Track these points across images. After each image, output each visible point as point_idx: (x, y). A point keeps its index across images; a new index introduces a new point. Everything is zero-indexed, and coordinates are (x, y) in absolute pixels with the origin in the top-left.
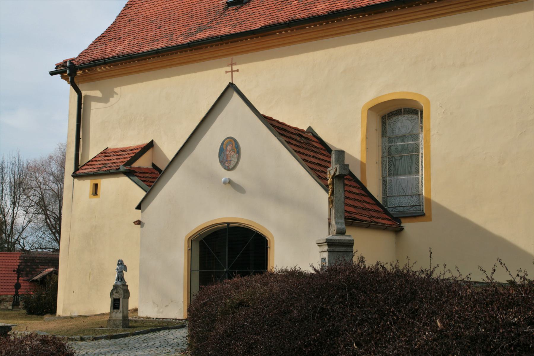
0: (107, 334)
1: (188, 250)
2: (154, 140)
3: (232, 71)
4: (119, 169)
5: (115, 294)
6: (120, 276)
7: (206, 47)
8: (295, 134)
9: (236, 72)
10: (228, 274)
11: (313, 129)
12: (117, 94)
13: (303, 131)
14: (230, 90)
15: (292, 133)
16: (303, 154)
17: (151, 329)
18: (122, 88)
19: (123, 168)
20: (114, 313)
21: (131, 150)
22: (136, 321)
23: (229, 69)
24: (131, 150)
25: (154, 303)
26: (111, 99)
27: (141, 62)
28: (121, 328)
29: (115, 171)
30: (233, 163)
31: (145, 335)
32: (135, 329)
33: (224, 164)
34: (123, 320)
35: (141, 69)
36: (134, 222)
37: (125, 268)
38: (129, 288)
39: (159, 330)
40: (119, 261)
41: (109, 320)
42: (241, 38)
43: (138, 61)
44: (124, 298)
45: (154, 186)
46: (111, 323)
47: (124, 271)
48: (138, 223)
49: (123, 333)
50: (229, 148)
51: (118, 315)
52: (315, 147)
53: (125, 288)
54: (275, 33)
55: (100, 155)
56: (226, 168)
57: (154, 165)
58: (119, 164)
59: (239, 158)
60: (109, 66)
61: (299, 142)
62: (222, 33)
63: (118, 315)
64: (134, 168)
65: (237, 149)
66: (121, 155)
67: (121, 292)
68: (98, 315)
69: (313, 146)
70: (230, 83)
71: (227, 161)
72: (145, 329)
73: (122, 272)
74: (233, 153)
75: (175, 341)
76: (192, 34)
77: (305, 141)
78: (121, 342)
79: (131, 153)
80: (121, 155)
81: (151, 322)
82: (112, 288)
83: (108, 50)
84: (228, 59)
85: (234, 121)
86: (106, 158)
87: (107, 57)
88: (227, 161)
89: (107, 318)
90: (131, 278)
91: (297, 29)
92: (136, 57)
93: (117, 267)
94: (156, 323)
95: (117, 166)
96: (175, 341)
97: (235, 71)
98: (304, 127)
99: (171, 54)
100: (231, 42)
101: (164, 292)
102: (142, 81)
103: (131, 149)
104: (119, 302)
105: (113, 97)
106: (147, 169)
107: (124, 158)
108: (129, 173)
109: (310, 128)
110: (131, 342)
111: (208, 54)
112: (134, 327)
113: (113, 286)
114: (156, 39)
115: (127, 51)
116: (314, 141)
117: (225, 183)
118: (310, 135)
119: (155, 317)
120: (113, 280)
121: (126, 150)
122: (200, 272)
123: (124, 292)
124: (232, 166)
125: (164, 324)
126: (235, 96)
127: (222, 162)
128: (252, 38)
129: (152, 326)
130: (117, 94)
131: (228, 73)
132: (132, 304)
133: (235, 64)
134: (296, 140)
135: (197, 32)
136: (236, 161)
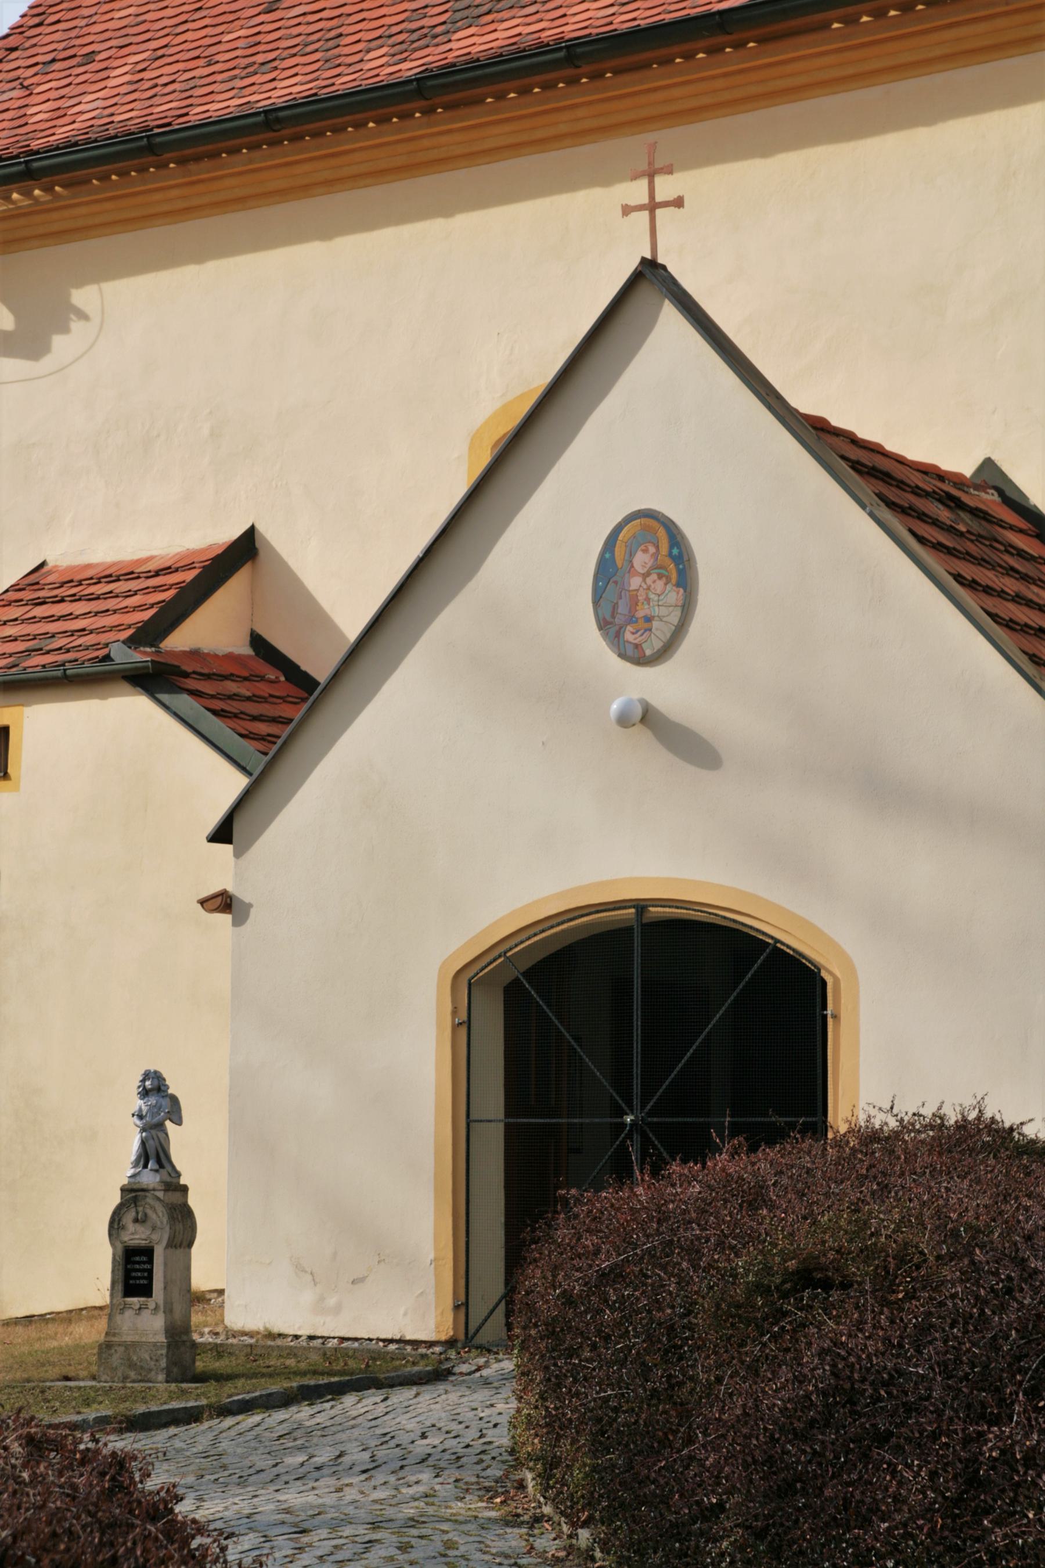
0: (105, 1410)
1: (456, 1027)
2: (260, 527)
3: (652, 206)
4: (107, 658)
5: (131, 1227)
6: (151, 1145)
7: (500, 97)
8: (927, 494)
9: (671, 209)
10: (644, 1136)
11: (1006, 468)
12: (83, 316)
13: (957, 480)
14: (646, 293)
15: (917, 491)
16: (988, 590)
17: (301, 1387)
18: (108, 287)
19: (125, 656)
20: (129, 1313)
21: (157, 574)
22: (219, 1351)
23: (637, 191)
24: (157, 574)
25: (299, 1268)
26: (58, 341)
27: (192, 167)
28: (160, 1385)
29: (88, 669)
30: (661, 631)
31: (281, 1415)
32: (228, 1387)
33: (618, 635)
34: (169, 1346)
35: (196, 201)
36: (203, 902)
37: (175, 1112)
38: (193, 1201)
39: (337, 1391)
40: (147, 1075)
41: (106, 1347)
42: (663, 52)
43: (181, 162)
44: (172, 1244)
45: (292, 736)
46: (116, 1359)
47: (168, 1124)
48: (223, 903)
49: (175, 1405)
50: (641, 560)
51: (148, 1324)
52: (1021, 554)
53: (175, 1197)
54: (826, 26)
55: (13, 596)
56: (630, 651)
57: (258, 642)
58: (104, 638)
59: (687, 608)
60: (48, 189)
61: (950, 530)
62: (571, 29)
63: (148, 1324)
64: (172, 653)
65: (678, 561)
66: (110, 595)
67: (159, 1215)
68: (17, 1321)
69: (1011, 549)
70: (644, 260)
71: (631, 619)
72: (275, 1387)
73: (160, 1126)
74: (660, 585)
75: (434, 1440)
76: (430, 36)
77: (976, 526)
78: (178, 1444)
79: (156, 589)
80: (110, 595)
81: (292, 1353)
82: (116, 1199)
83: (39, 113)
84: (632, 146)
85: (665, 436)
86: (39, 611)
87: (35, 145)
88: (631, 619)
89: (91, 1333)
90: (197, 1152)
91: (760, 41)
92: (167, 146)
93: (138, 1103)
94: (314, 1357)
95: (96, 646)
96: (434, 1440)
97: (666, 204)
98: (966, 466)
99: (335, 130)
100: (617, 72)
101: (349, 1220)
102: (199, 258)
103: (152, 566)
104: (151, 1261)
105: (65, 330)
106: (230, 657)
107: (125, 610)
108: (156, 680)
109: (988, 465)
110: (224, 1445)
111: (507, 128)
112: (220, 1378)
113: (123, 1190)
114: (260, 58)
115: (129, 116)
116: (1011, 528)
117: (623, 720)
118: (992, 496)
119: (304, 1332)
120: (118, 1163)
121: (130, 575)
122: (508, 1127)
123: (172, 1219)
124: (658, 645)
125: (352, 1364)
126: (670, 315)
127: (609, 626)
128: (142, 170)
129: (304, 1374)
130: (83, 316)
131: (634, 215)
132: (205, 1269)
133: (669, 170)
134: (936, 523)
135: (450, 28)
136: (675, 618)
